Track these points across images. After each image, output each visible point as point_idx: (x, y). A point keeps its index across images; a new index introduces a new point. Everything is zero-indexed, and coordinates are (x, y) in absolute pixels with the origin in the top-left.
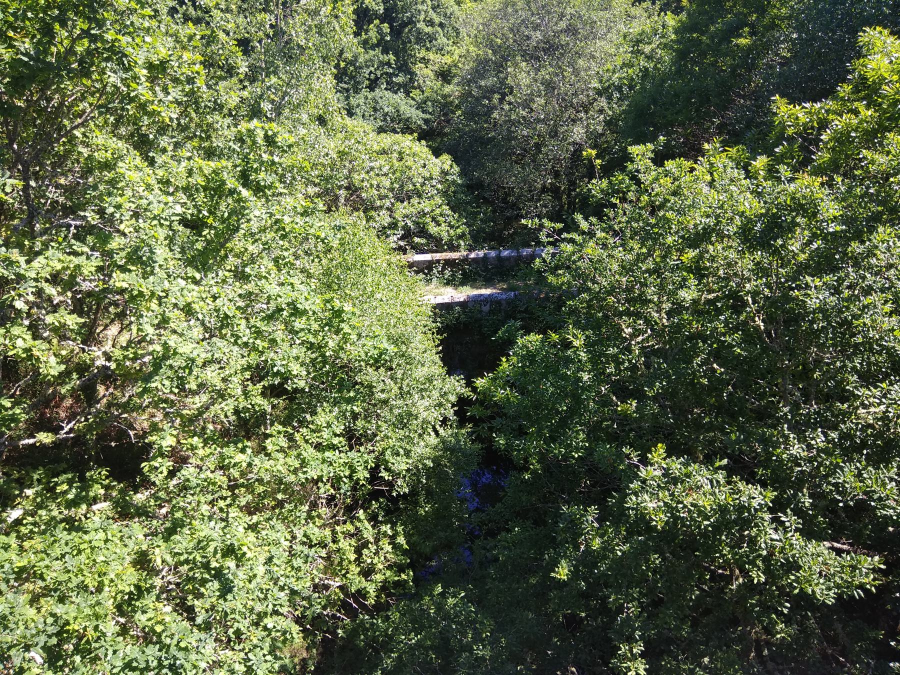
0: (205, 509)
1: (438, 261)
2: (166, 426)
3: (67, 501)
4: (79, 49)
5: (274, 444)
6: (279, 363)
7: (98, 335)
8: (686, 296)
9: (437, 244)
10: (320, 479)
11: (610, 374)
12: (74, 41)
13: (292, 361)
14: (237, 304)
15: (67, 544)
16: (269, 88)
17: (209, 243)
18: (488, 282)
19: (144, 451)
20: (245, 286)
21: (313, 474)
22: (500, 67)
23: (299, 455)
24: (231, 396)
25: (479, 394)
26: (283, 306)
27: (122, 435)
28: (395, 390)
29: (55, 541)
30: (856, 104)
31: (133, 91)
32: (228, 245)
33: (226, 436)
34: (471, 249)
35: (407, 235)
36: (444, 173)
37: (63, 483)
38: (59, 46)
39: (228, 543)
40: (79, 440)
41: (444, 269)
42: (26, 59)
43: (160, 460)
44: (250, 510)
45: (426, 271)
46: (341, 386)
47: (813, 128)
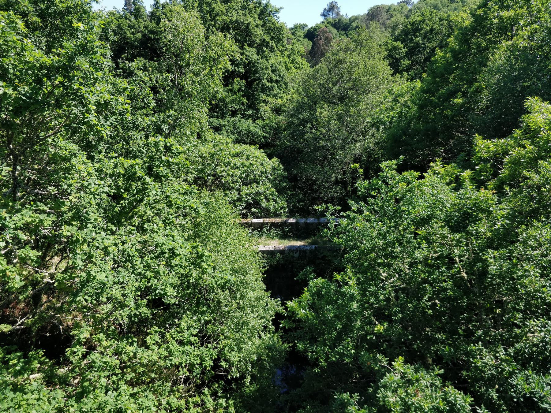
0: (103, 381)
1: (267, 223)
2: (84, 324)
3: (15, 371)
4: (57, 92)
5: (152, 340)
6: (160, 287)
7: (47, 262)
8: (419, 255)
9: (266, 213)
10: (180, 364)
11: (372, 304)
12: (54, 87)
15: (12, 401)
16: (168, 117)
17: (123, 208)
18: (298, 237)
19: (68, 340)
21: (175, 361)
22: (312, 108)
23: (168, 347)
24: (127, 306)
27: (55, 328)
28: (235, 306)
29: (5, 398)
30: (525, 141)
31: (87, 118)
32: (135, 210)
33: (122, 333)
34: (289, 217)
35: (249, 206)
37: (14, 359)
38: (45, 90)
39: (119, 407)
40: (27, 331)
41: (270, 228)
42: (24, 98)
43: (78, 347)
44: (131, 384)
47: (499, 154)
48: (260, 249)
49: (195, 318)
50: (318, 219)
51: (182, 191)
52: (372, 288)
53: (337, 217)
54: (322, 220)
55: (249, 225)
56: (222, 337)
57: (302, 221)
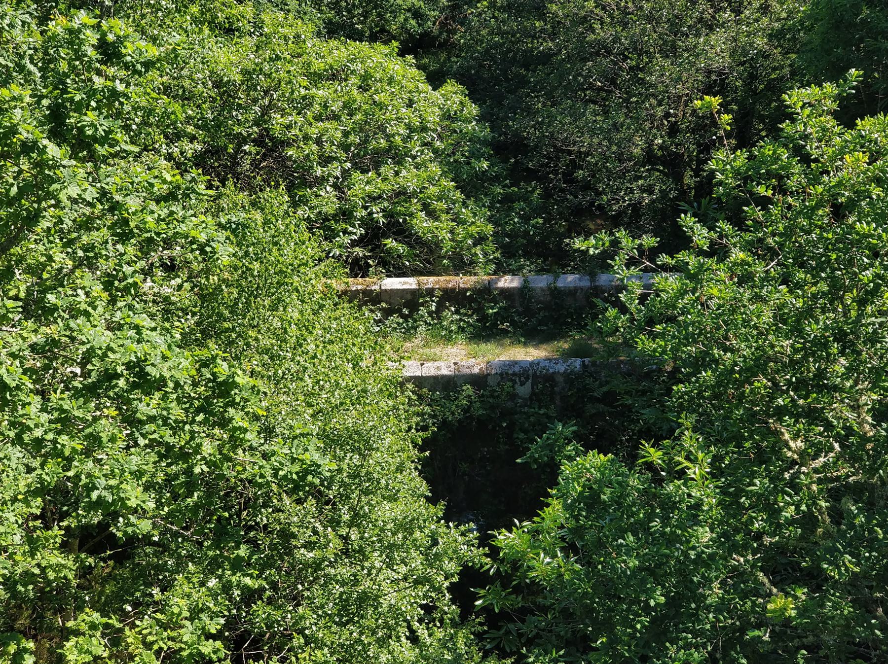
1: (430, 292)
5: (80, 652)
9: (428, 256)
11: (758, 536)
13: (126, 480)
14: (28, 364)
18: (531, 335)
20: (43, 329)
25: (502, 561)
26: (119, 369)
28: (335, 544)
34: (501, 269)
35: (372, 236)
36: (448, 116)
41: (441, 307)
45: (406, 311)
46: (221, 535)
48: (408, 373)
49: (213, 583)
50: (593, 276)
51: (159, 188)
52: (758, 485)
53: (646, 270)
54: (603, 279)
55: (372, 298)
56: (298, 641)
57: (541, 282)
